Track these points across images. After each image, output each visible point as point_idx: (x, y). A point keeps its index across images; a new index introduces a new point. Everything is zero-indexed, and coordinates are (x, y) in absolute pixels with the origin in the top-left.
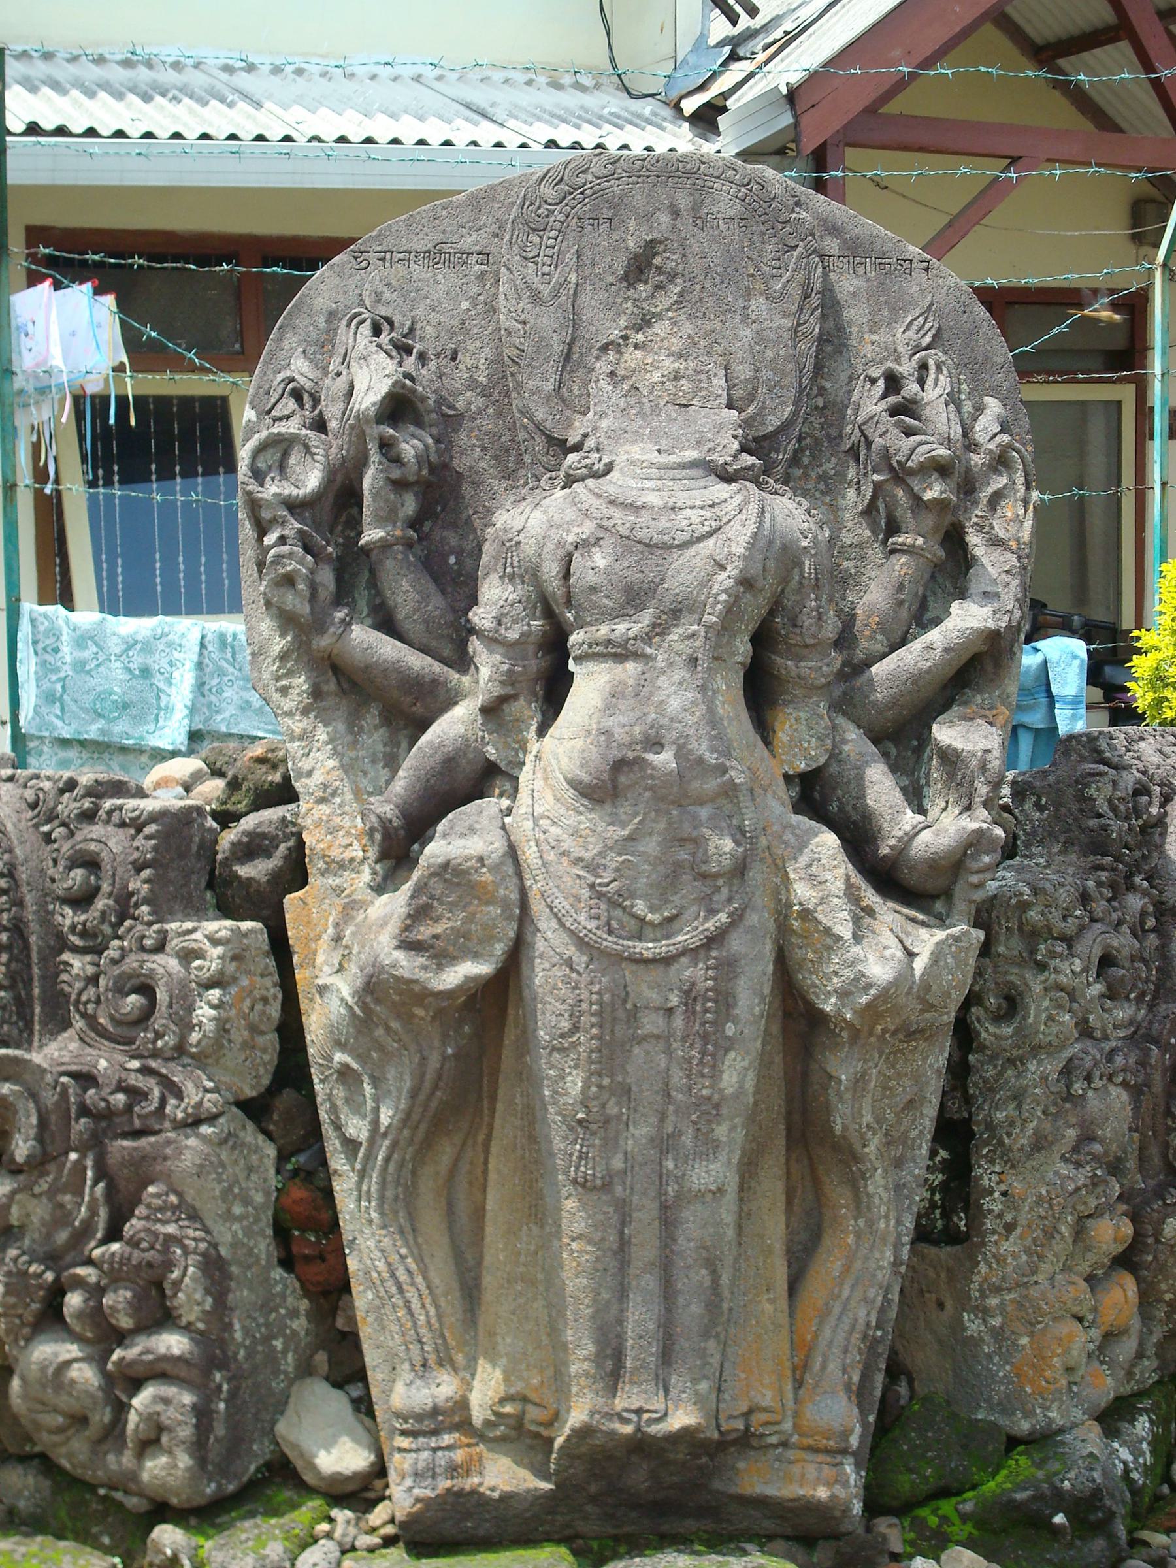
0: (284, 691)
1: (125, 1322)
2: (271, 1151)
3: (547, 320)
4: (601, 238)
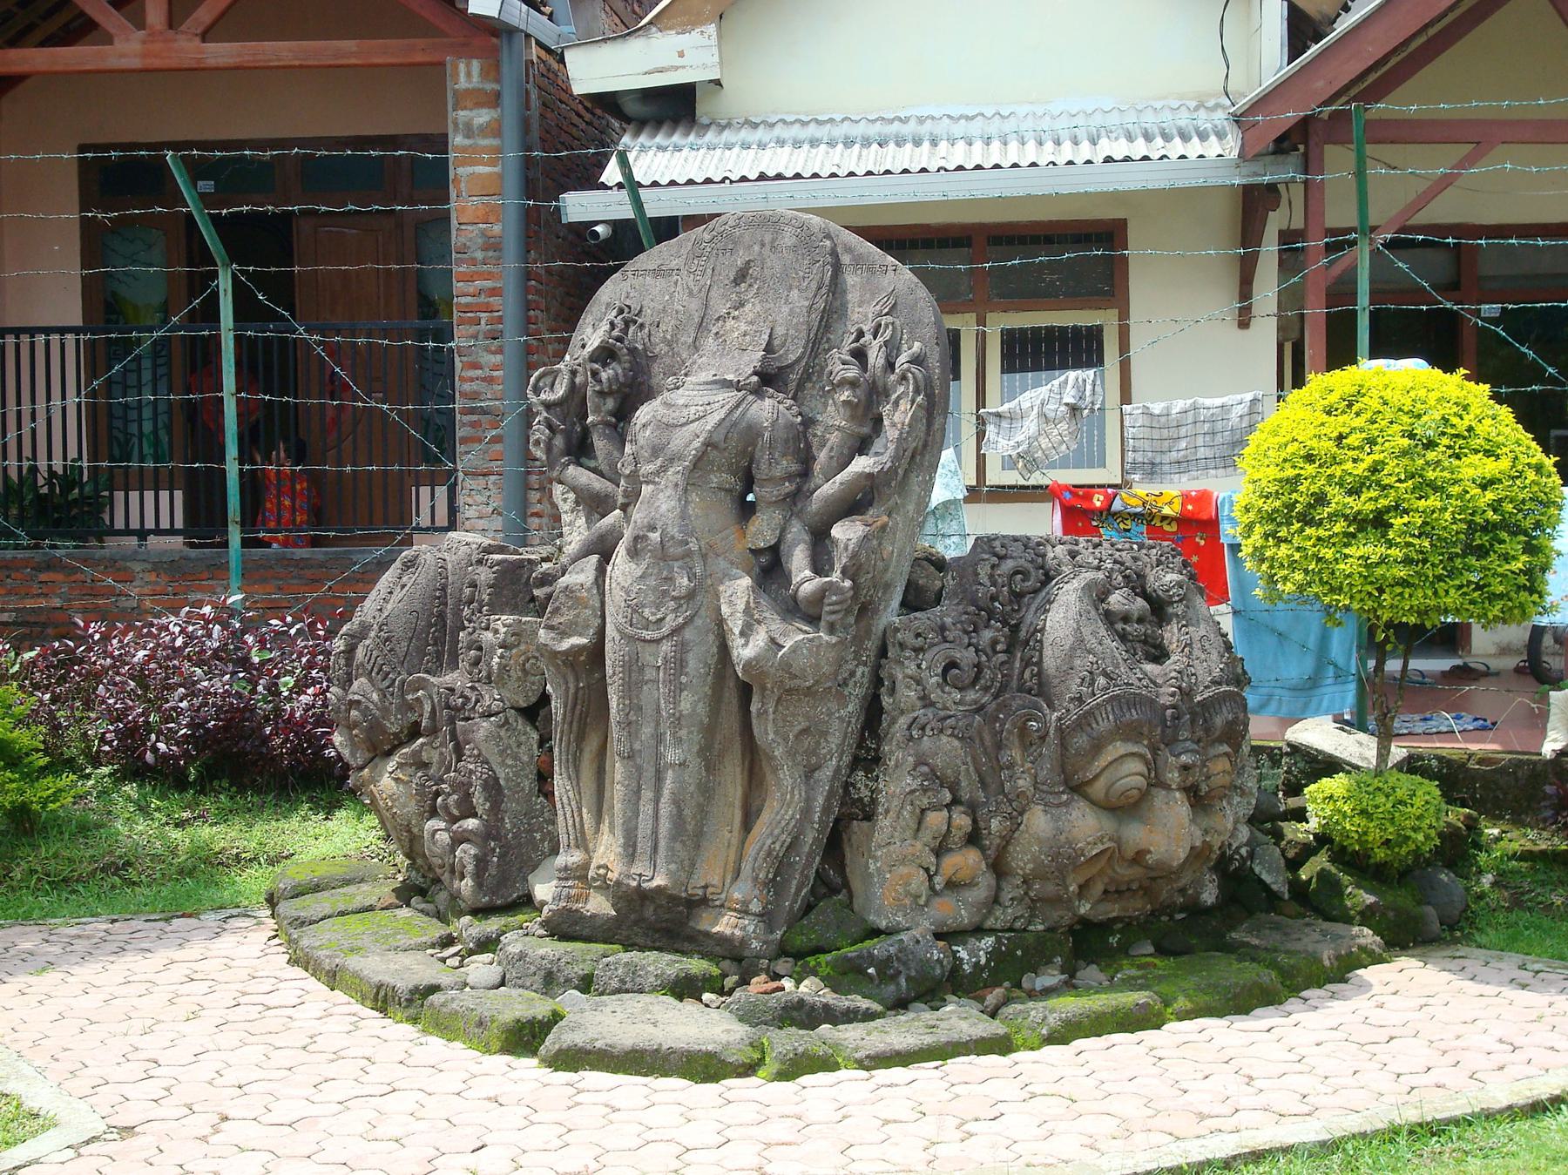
0: (565, 500)
1: (456, 812)
2: (535, 736)
3: (695, 305)
4: (726, 260)
